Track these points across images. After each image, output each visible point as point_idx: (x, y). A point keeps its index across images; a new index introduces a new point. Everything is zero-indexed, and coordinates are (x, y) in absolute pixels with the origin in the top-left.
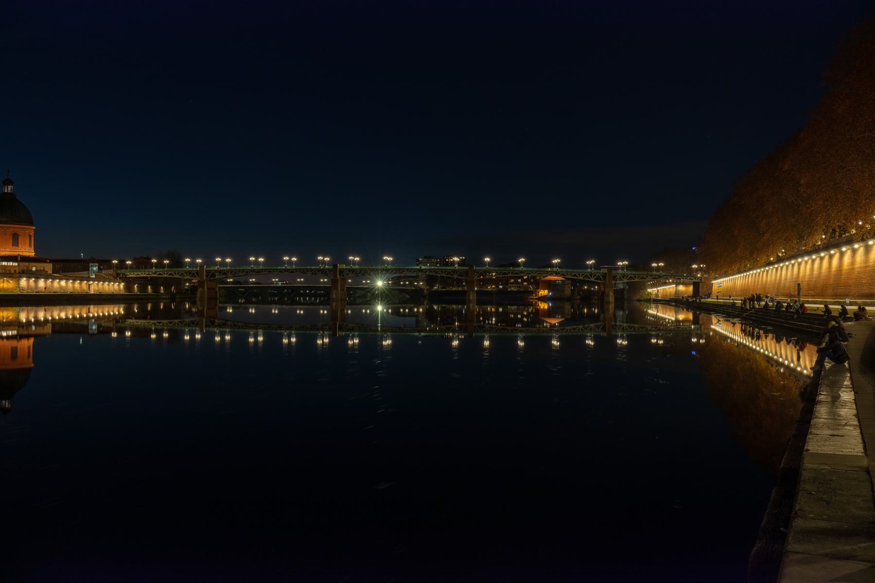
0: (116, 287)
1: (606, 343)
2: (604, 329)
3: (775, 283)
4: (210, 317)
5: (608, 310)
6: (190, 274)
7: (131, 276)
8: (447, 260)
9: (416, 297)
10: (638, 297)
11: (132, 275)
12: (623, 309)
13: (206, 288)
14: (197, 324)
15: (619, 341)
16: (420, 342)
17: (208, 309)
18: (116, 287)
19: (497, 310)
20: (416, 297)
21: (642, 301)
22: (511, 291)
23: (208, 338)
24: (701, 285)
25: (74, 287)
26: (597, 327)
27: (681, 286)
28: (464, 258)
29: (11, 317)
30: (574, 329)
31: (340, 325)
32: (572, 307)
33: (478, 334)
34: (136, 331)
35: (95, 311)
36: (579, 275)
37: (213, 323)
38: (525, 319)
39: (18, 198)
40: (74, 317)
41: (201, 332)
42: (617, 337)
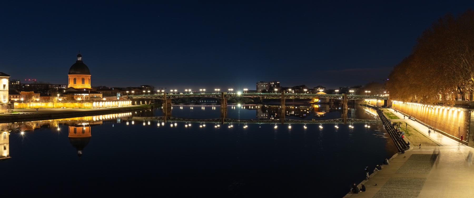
0: (127, 104)
1: (344, 127)
2: (343, 121)
3: (411, 110)
4: (168, 115)
5: (345, 112)
6: (159, 97)
7: (134, 98)
8: (271, 84)
9: (257, 101)
10: (361, 103)
11: (134, 98)
12: (354, 108)
13: (166, 103)
14: (163, 119)
15: (350, 126)
16: (260, 127)
17: (167, 112)
18: (127, 104)
19: (295, 108)
20: (257, 101)
21: (362, 105)
22: (301, 99)
23: (167, 125)
24: (388, 101)
25: (112, 105)
26: (340, 120)
27: (379, 100)
28: (279, 82)
29: (90, 119)
30: (329, 121)
31: (225, 119)
32: (330, 107)
33: (286, 123)
34: (136, 121)
35: (120, 115)
36: (332, 97)
37: (170, 118)
38: (308, 112)
39: (84, 63)
40: (113, 118)
41: (165, 122)
42: (349, 124)
